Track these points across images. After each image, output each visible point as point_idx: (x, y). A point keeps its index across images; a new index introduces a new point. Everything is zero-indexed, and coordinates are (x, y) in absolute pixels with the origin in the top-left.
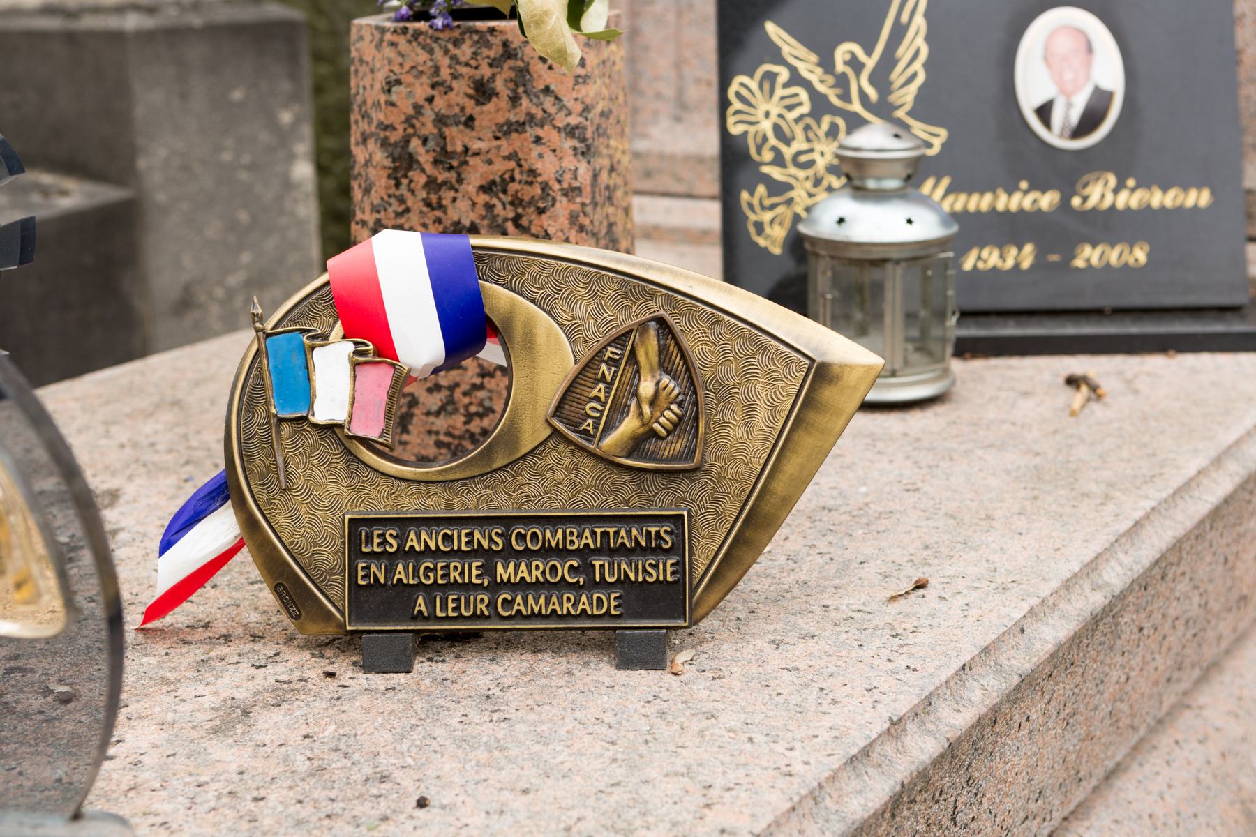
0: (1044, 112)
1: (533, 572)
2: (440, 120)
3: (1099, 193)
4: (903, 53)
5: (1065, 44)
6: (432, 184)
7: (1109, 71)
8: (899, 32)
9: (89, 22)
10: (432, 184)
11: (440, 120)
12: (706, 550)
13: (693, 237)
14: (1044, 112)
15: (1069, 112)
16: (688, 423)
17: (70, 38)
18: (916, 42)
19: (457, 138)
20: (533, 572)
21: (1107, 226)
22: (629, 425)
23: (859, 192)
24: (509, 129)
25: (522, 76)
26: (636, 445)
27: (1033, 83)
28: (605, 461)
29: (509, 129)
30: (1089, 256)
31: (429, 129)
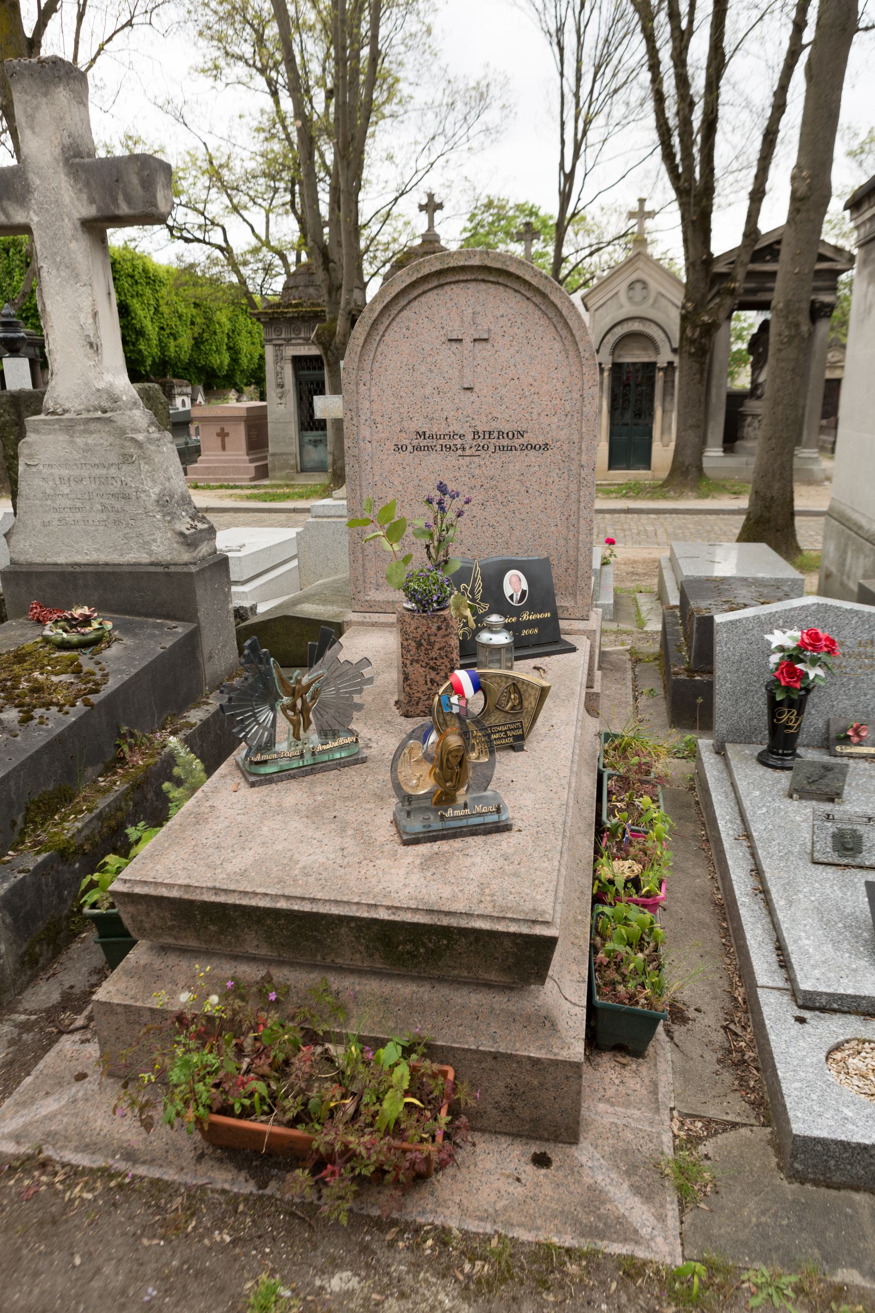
0: (511, 597)
1: (497, 736)
2: (429, 635)
3: (525, 617)
4: (477, 585)
5: (514, 579)
6: (426, 649)
7: (525, 586)
8: (475, 579)
9: (173, 569)
10: (426, 649)
11: (429, 635)
12: (526, 725)
13: (392, 625)
14: (511, 597)
15: (517, 597)
16: (521, 702)
17: (168, 574)
18: (479, 582)
19: (433, 639)
20: (497, 736)
21: (530, 624)
22: (510, 704)
23: (492, 632)
24: (444, 636)
25: (448, 625)
26: (512, 708)
27: (508, 590)
28: (507, 712)
29: (444, 636)
30: (525, 632)
31: (426, 637)
